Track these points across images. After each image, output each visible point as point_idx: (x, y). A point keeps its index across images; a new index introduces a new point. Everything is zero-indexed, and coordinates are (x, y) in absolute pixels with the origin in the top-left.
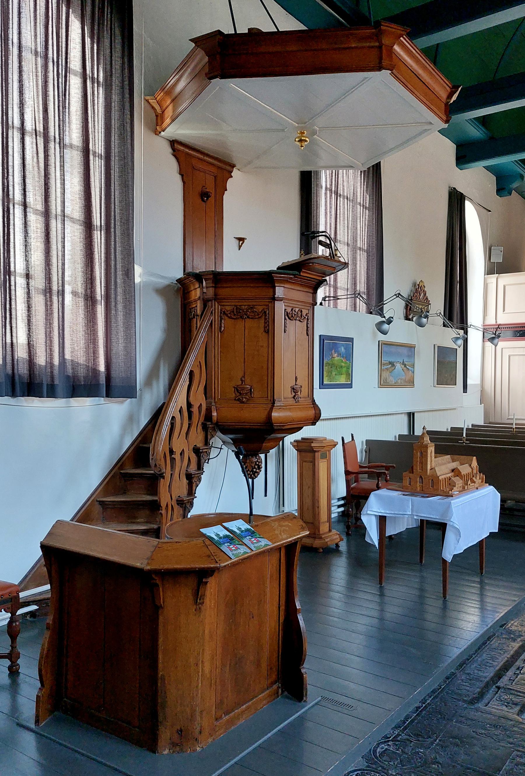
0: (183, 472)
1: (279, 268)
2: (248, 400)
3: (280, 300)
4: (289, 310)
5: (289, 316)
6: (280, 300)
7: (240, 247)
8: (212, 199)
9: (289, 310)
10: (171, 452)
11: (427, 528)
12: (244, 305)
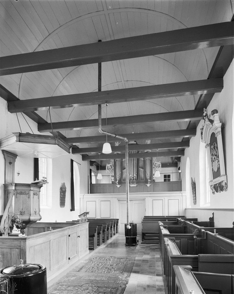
0: (7, 233)
1: (32, 183)
2: (24, 214)
3: (32, 190)
4: (34, 193)
5: (34, 194)
6: (32, 190)
7: (18, 175)
8: (12, 164)
9: (34, 193)
10: (5, 228)
11: (214, 227)
12: (23, 191)
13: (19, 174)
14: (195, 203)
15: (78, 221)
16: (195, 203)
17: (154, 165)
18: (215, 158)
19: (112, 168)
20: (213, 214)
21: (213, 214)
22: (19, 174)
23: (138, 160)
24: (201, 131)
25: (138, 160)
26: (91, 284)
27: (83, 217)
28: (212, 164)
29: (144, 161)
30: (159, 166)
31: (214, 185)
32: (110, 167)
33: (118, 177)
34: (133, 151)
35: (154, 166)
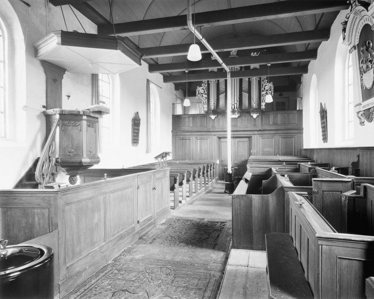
13: (69, 96)
14: (325, 138)
15: (153, 165)
16: (325, 138)
17: (263, 87)
18: (368, 67)
19: (204, 92)
20: (358, 156)
21: (358, 156)
22: (69, 96)
23: (241, 81)
24: (343, 26)
25: (241, 81)
26: (166, 268)
27: (160, 159)
28: (362, 77)
29: (250, 83)
30: (271, 89)
31: (364, 111)
32: (202, 91)
33: (213, 104)
34: (234, 78)
35: (263, 89)
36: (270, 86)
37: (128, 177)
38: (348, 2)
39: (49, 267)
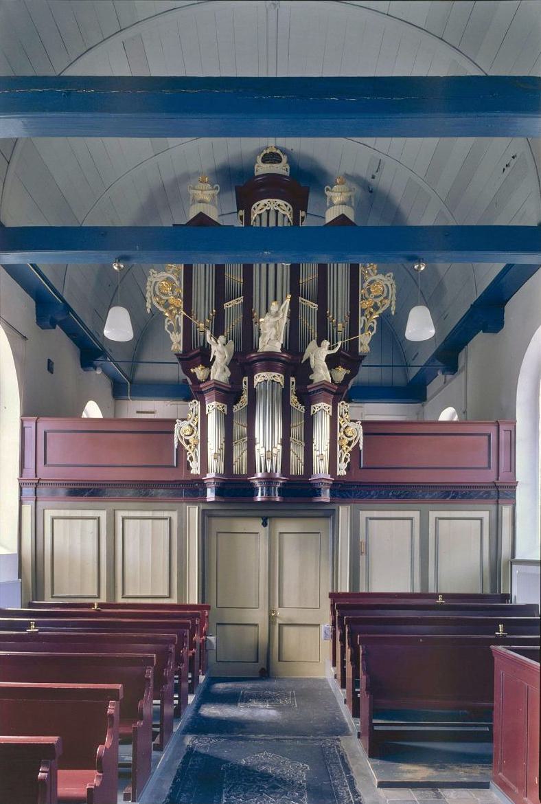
36: (386, 285)
37: (342, 515)
38: (421, 640)
39: (207, 617)
